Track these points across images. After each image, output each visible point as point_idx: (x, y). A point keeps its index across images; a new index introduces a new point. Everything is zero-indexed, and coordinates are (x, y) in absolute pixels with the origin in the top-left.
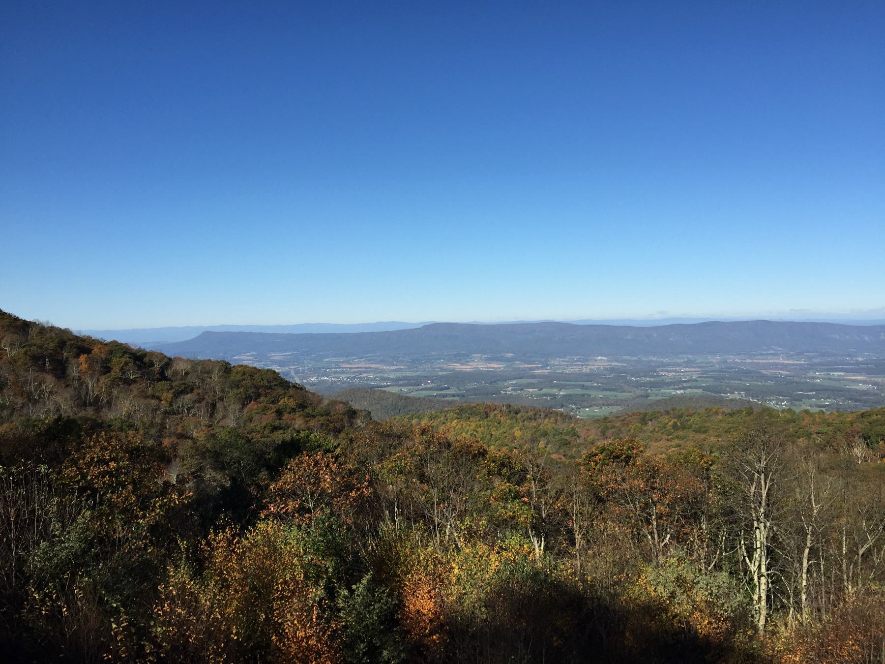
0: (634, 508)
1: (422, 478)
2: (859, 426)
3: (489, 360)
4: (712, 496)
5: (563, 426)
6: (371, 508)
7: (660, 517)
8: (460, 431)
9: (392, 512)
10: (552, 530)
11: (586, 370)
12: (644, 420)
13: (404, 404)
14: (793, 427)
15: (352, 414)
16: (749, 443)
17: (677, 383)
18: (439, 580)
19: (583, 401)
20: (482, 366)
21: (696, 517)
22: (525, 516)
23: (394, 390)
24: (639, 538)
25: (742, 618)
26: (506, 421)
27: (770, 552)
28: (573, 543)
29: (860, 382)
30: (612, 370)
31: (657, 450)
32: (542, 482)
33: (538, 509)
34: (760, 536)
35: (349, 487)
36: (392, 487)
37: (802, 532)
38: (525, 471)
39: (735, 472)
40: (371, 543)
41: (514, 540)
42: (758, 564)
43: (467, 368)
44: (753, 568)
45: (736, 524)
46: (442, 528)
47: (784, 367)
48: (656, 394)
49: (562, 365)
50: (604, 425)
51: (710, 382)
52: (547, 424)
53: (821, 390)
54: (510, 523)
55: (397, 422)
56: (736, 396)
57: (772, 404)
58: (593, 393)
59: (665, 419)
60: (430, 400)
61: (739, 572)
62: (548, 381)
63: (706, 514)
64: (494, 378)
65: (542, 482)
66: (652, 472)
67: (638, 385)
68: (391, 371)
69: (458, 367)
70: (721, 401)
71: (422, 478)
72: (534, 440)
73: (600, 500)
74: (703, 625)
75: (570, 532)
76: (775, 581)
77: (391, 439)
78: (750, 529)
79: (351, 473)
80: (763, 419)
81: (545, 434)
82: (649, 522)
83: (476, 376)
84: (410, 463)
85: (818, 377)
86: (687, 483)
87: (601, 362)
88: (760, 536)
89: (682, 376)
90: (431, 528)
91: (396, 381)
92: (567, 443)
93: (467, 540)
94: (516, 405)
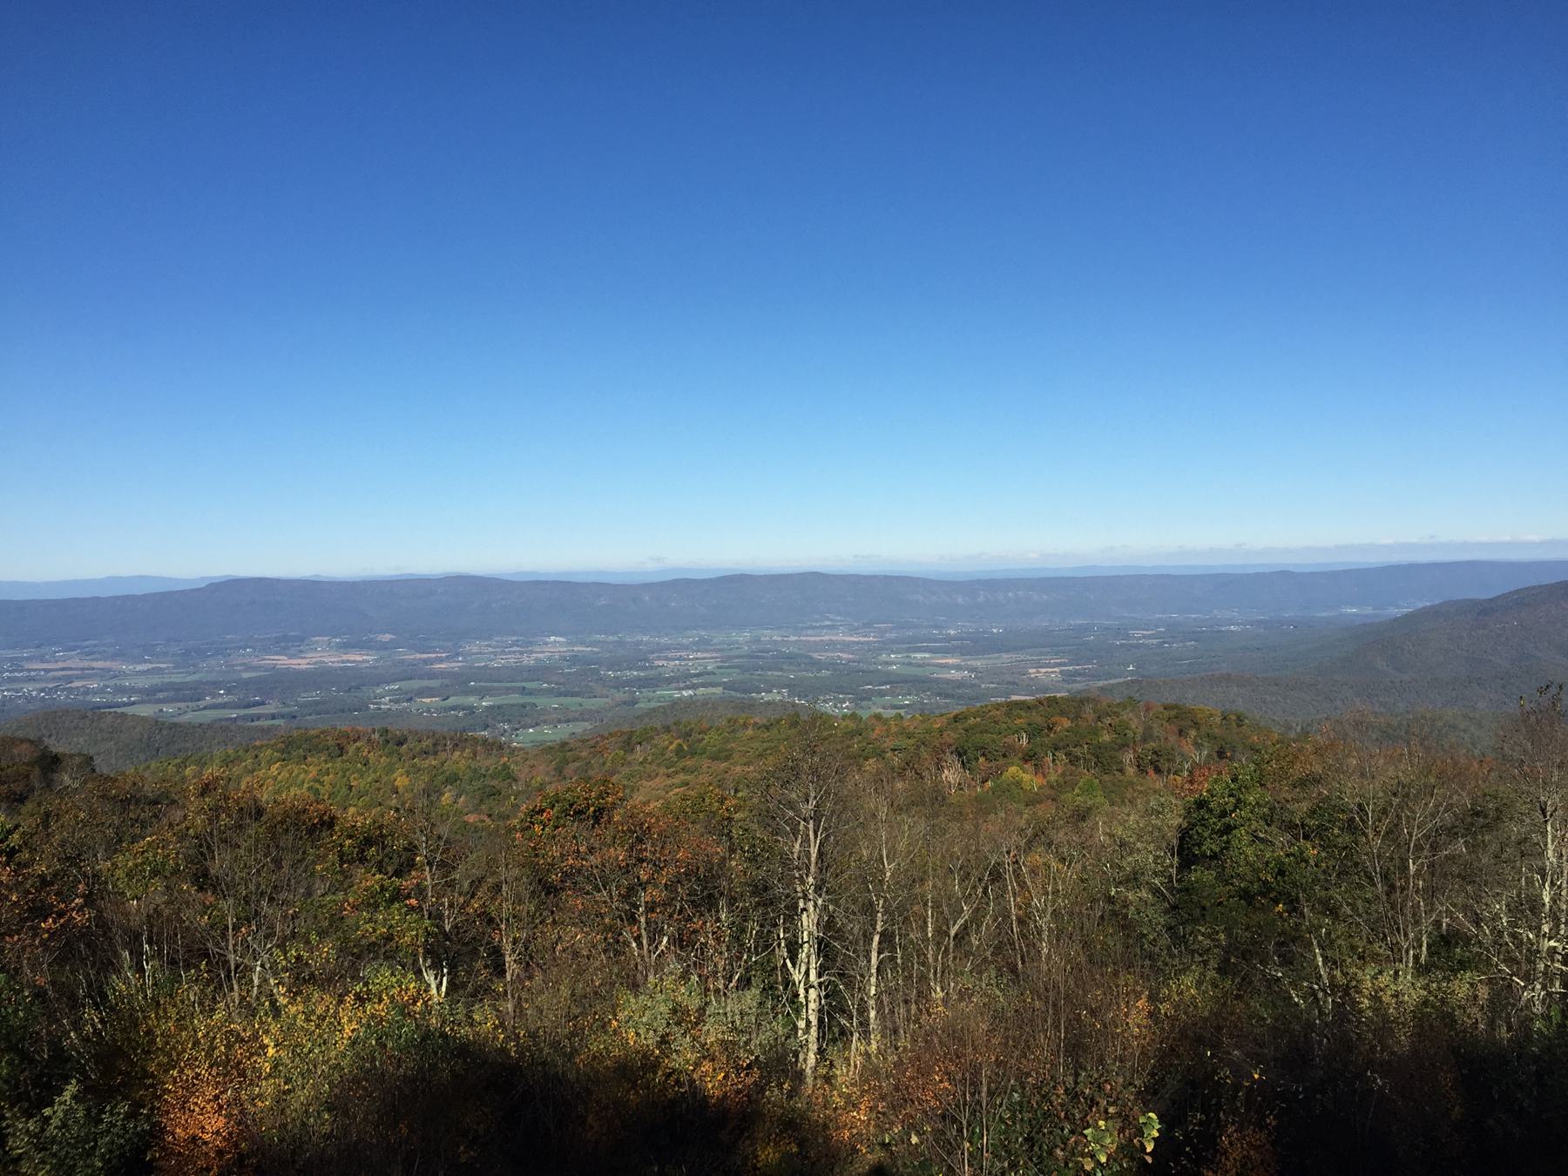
0: (608, 899)
1: (203, 880)
2: (951, 736)
3: (347, 647)
5: (488, 763)
6: (90, 949)
7: (651, 908)
8: (283, 784)
9: (137, 954)
10: (463, 953)
11: (528, 660)
12: (628, 745)
13: (166, 738)
14: (857, 743)
15: (51, 763)
17: (682, 679)
18: (234, 1070)
19: (522, 715)
20: (332, 659)
21: (710, 902)
22: (411, 934)
23: (146, 711)
24: (616, 948)
25: (781, 1064)
26: (379, 759)
27: (823, 948)
28: (500, 970)
29: (952, 667)
30: (575, 660)
31: (652, 794)
32: (446, 867)
33: (437, 917)
34: (808, 923)
35: (41, 912)
36: (139, 903)
37: (869, 909)
38: (412, 849)
39: (768, 818)
40: (90, 1015)
41: (382, 977)
42: (806, 972)
43: (301, 664)
44: (797, 976)
45: (773, 905)
46: (244, 972)
47: (846, 646)
48: (650, 699)
49: (484, 653)
50: (561, 754)
51: (736, 675)
52: (458, 761)
53: (900, 682)
54: (385, 949)
55: (150, 774)
56: (774, 696)
57: (828, 707)
58: (541, 701)
59: (663, 740)
60: (223, 729)
61: (779, 993)
62: (460, 682)
63: (721, 897)
64: (355, 680)
65: (446, 867)
66: (638, 834)
67: (619, 684)
68: (137, 672)
69: (283, 661)
70: (751, 706)
71: (203, 880)
72: (432, 792)
73: (551, 890)
74: (713, 1081)
75: (497, 953)
76: (831, 993)
77: (135, 808)
78: (793, 913)
79: (44, 882)
80: (806, 727)
81: (453, 779)
82: (633, 920)
83: (319, 678)
84: (175, 852)
85: (894, 661)
86: (695, 846)
87: (554, 646)
88: (808, 923)
89: (691, 665)
90: (221, 975)
91: (149, 694)
92: (494, 793)
93: (294, 994)
94: (397, 729)
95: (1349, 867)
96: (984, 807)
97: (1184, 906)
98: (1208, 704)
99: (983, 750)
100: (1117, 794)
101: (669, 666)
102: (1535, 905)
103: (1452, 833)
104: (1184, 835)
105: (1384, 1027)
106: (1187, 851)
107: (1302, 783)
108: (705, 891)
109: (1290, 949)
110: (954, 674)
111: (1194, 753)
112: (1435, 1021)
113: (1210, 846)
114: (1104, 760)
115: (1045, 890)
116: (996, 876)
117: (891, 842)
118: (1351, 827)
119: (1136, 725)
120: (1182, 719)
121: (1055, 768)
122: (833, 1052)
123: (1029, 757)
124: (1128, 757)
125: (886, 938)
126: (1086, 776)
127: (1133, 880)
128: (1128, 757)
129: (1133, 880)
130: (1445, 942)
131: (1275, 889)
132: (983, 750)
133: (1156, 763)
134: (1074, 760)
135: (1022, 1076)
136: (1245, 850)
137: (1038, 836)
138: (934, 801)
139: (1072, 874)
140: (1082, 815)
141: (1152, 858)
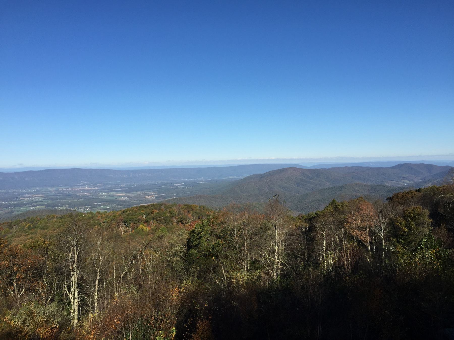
2: (122, 217)
4: (49, 263)
12: (10, 226)
14: (91, 221)
16: (69, 231)
21: (40, 276)
29: (122, 196)
34: (74, 279)
37: (95, 272)
44: (70, 296)
45: (62, 274)
47: (88, 191)
48: (18, 211)
51: (50, 202)
53: (105, 202)
56: (64, 208)
61: (63, 301)
66: (13, 256)
67: (6, 206)
70: (56, 211)
76: (82, 300)
78: (69, 276)
82: (11, 284)
85: (104, 195)
88: (74, 279)
96: (132, 237)
97: (188, 261)
98: (195, 204)
99: (132, 221)
100: (170, 231)
101: (25, 199)
102: (274, 251)
103: (255, 234)
104: (189, 241)
105: (240, 287)
106: (189, 246)
107: (219, 224)
108: (38, 272)
110: (123, 199)
111: (192, 217)
112: (250, 284)
113: (195, 243)
114: (167, 221)
115: (150, 259)
116: (135, 258)
117: (101, 251)
118: (231, 235)
119: (176, 210)
120: (189, 208)
121: (154, 224)
122: (83, 318)
123: (146, 222)
124: (174, 220)
125: (101, 281)
126: (162, 226)
127: (175, 255)
128: (174, 220)
129: (175, 255)
130: (254, 262)
131: (212, 253)
132: (132, 221)
133: (182, 221)
134: (159, 222)
135: (142, 316)
136: (204, 244)
137: (148, 245)
138: (117, 237)
139: (157, 255)
140: (161, 237)
141: (180, 248)
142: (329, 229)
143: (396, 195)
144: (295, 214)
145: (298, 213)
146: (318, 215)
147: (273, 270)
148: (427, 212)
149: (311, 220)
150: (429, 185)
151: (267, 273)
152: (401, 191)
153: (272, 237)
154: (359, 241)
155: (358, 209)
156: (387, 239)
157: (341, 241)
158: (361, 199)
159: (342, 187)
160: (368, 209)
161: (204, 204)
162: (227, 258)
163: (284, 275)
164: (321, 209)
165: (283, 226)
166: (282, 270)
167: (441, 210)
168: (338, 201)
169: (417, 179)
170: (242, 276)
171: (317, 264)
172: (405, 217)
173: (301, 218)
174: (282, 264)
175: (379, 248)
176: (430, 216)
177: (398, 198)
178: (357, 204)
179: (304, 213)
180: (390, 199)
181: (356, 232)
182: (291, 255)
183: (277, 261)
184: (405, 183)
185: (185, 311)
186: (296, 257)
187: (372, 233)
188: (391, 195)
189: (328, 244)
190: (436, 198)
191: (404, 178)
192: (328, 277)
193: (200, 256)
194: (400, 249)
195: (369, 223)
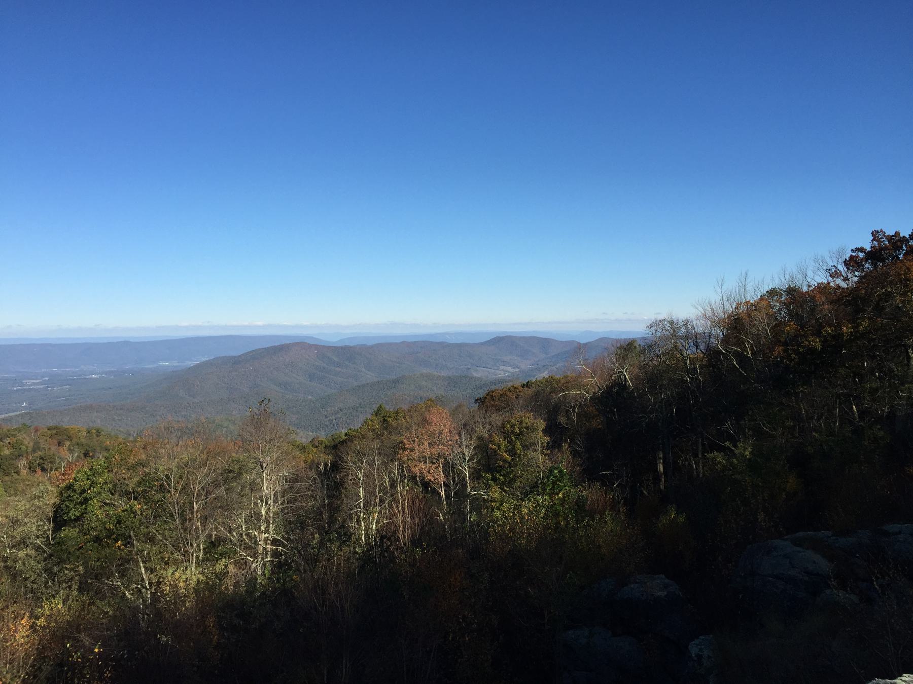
95: (159, 512)
97: (55, 554)
98: (78, 424)
102: (258, 516)
103: (216, 485)
104: (57, 509)
106: (59, 520)
107: (134, 467)
109: (125, 566)
111: (67, 455)
112: (207, 592)
113: (74, 513)
119: (27, 441)
120: (60, 435)
124: (23, 463)
127: (23, 543)
128: (23, 463)
129: (23, 543)
130: (213, 545)
131: (117, 533)
133: (42, 465)
136: (97, 513)
142: (371, 463)
143: (490, 395)
144: (303, 437)
145: (311, 435)
146: (349, 438)
147: (255, 556)
148: (541, 424)
149: (337, 447)
150: (545, 374)
151: (242, 564)
152: (499, 387)
153: (255, 487)
154: (426, 485)
155: (425, 422)
156: (476, 475)
157: (393, 485)
158: (431, 403)
159: (396, 382)
160: (442, 423)
161: (99, 424)
162: (151, 540)
163: (280, 566)
164: (357, 425)
165: (277, 463)
166: (275, 554)
167: (562, 420)
168: (389, 408)
169: (526, 365)
170: (185, 577)
171: (346, 536)
172: (507, 435)
173: (315, 443)
174: (274, 542)
175: (461, 494)
176: (546, 431)
177: (492, 400)
178: (421, 412)
179: (323, 436)
180: (480, 401)
181: (419, 468)
182: (294, 523)
183: (265, 537)
184: (506, 372)
185: (47, 668)
186: (303, 526)
187: (449, 467)
188: (481, 393)
189: (370, 493)
190: (556, 397)
191: (505, 363)
192: (367, 559)
193: (85, 541)
194: (496, 493)
195: (441, 447)
